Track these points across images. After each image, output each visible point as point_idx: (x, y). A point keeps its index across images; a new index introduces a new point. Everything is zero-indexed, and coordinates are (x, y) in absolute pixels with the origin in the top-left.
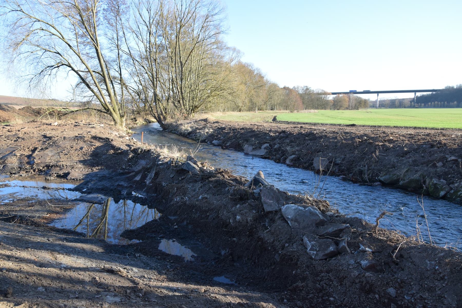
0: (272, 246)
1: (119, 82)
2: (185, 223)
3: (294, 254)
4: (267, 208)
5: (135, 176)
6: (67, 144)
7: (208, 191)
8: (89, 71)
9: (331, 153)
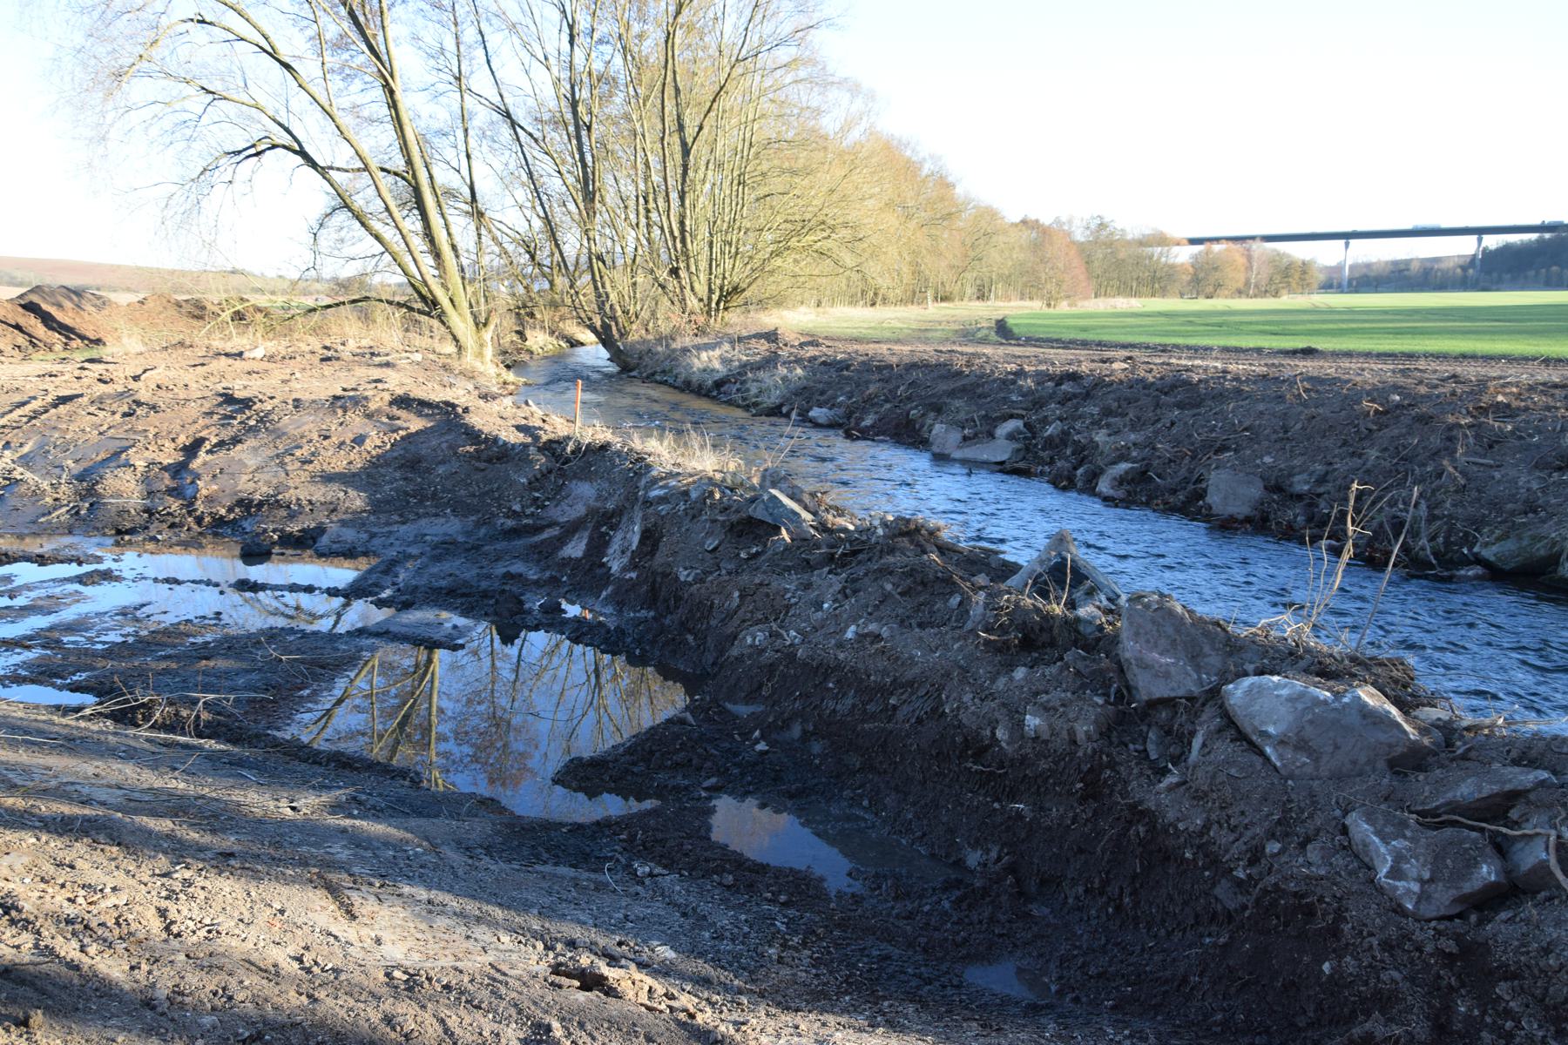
0: (1200, 847)
1: (467, 208)
2: (796, 731)
3: (1319, 891)
4: (1148, 687)
5: (562, 540)
6: (309, 425)
7: (877, 607)
8: (366, 168)
9: (1269, 453)
